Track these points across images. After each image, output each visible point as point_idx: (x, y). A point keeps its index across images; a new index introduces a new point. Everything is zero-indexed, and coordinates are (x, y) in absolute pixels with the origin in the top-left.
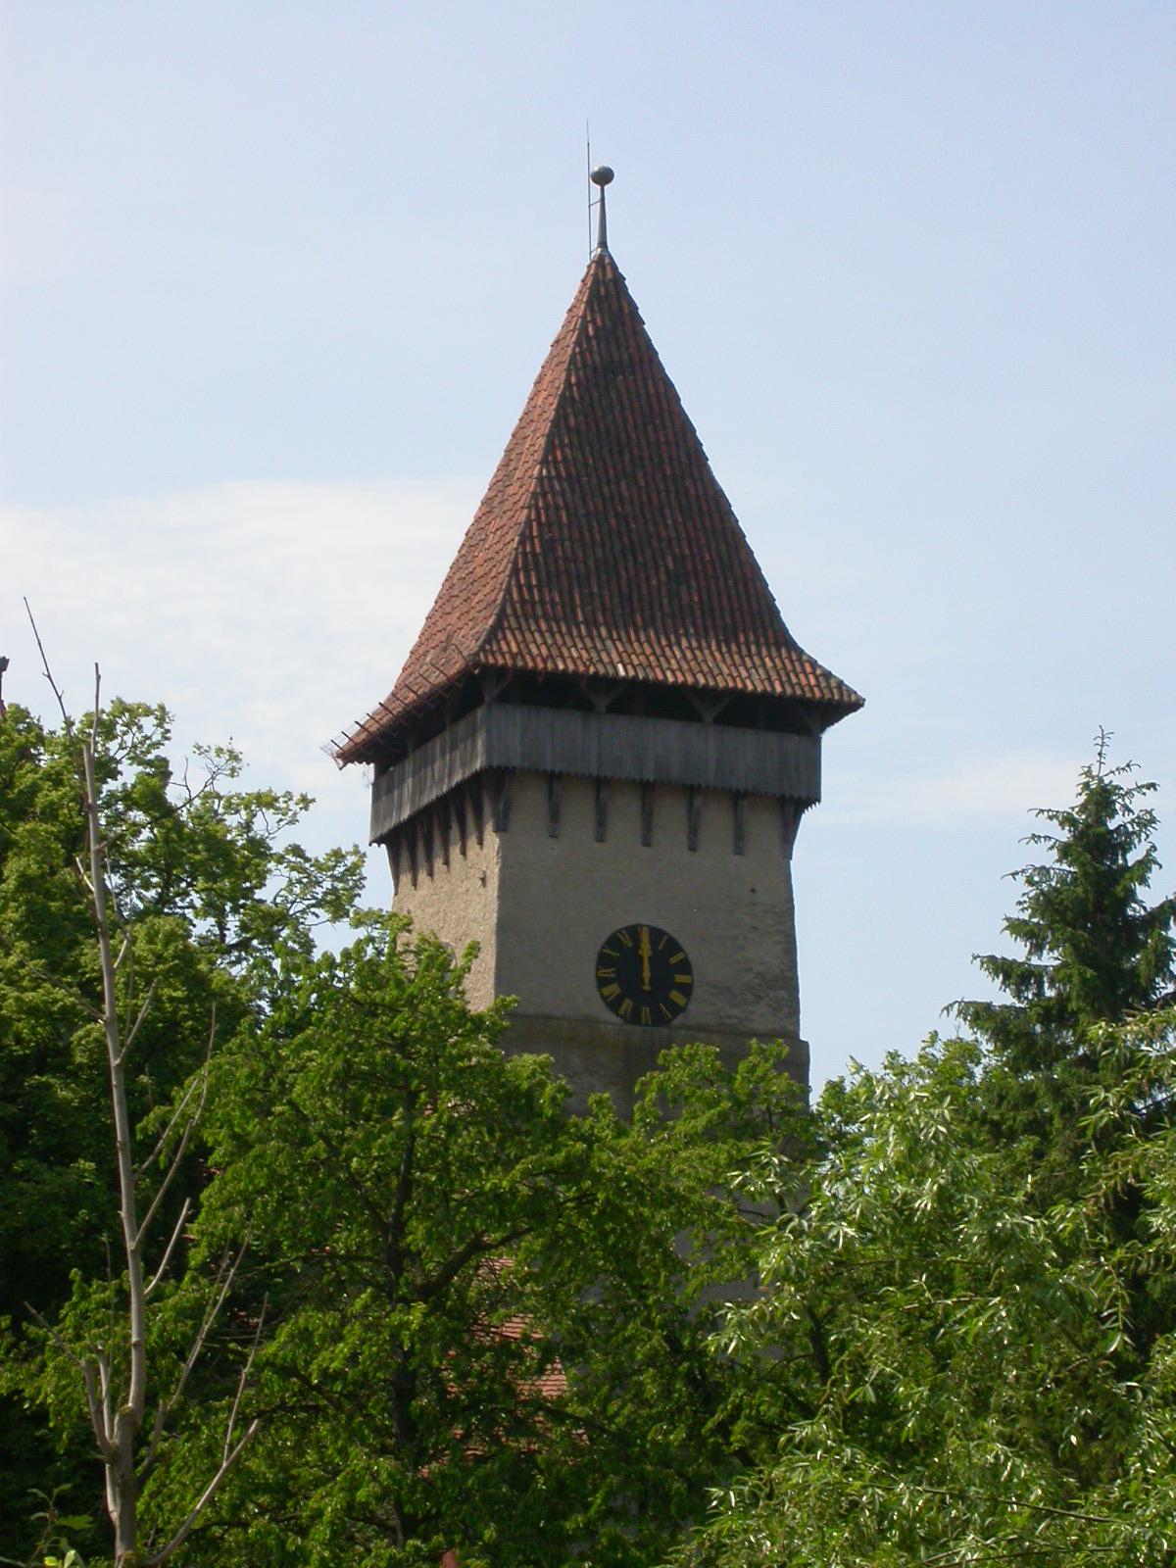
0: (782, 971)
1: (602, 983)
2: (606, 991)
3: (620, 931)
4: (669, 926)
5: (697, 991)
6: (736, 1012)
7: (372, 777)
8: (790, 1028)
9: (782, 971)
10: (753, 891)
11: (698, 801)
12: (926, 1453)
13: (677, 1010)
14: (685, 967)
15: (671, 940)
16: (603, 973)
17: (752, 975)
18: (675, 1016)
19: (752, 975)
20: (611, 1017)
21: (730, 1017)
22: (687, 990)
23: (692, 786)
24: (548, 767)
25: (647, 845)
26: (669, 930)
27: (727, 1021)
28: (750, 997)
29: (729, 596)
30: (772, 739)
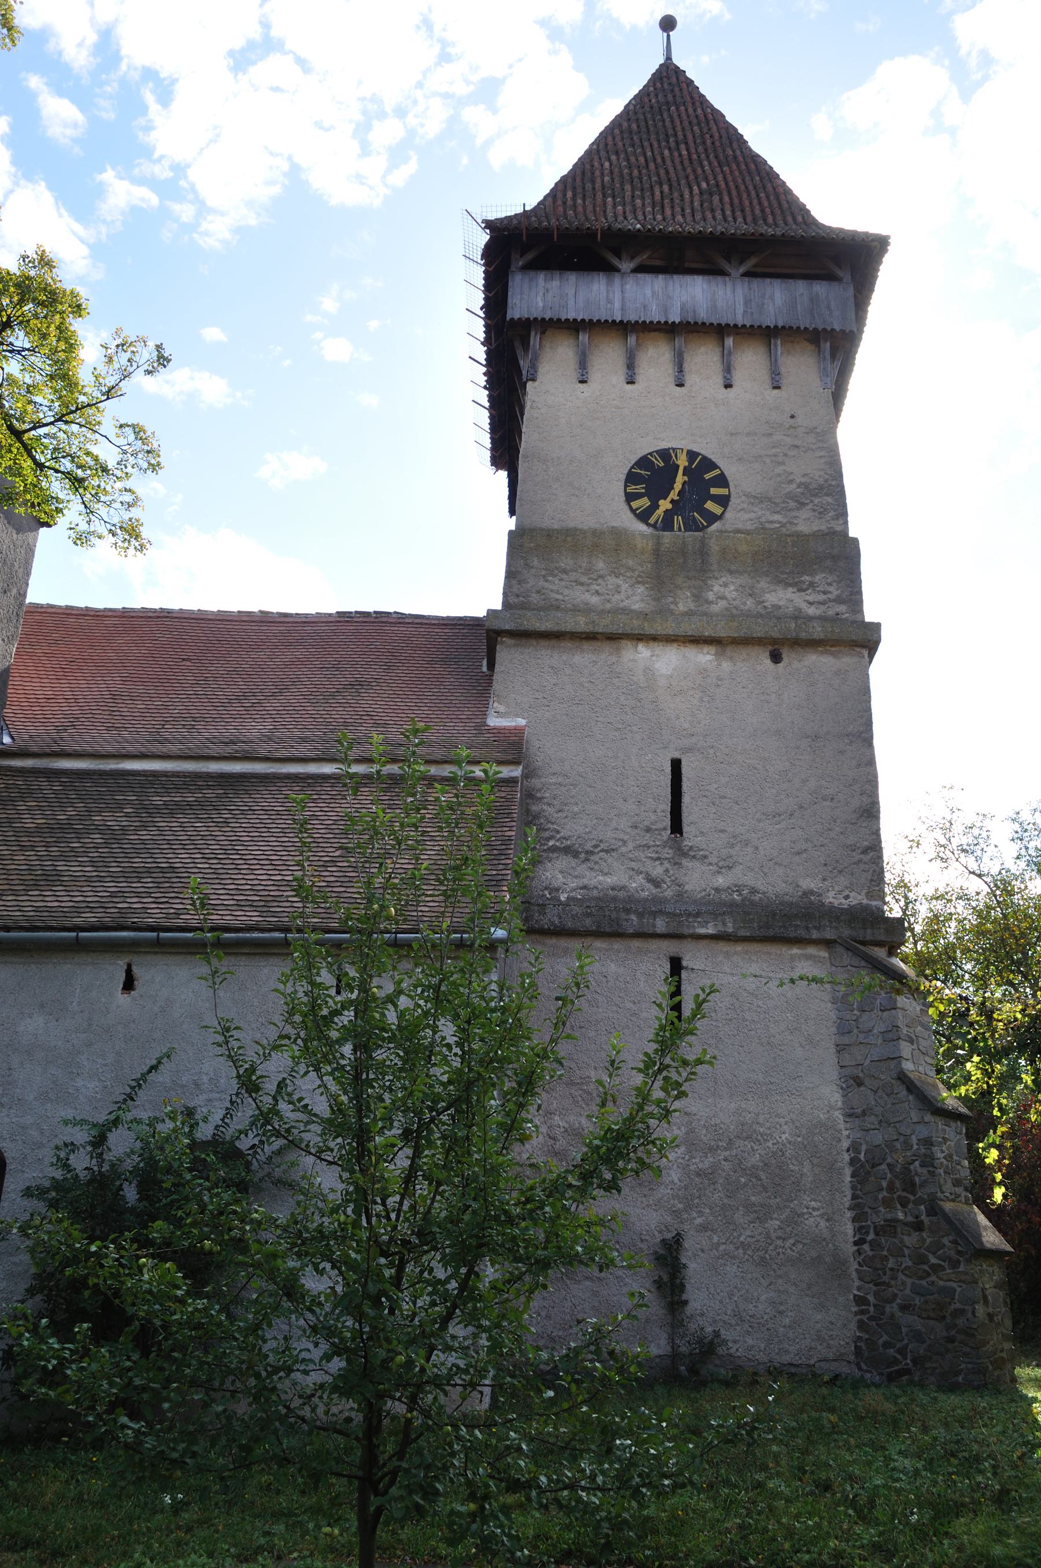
0: (826, 481)
1: (630, 498)
2: (634, 505)
3: (651, 454)
4: (707, 449)
5: (734, 501)
6: (776, 517)
7: (47, 198)
8: (839, 529)
9: (826, 481)
10: (792, 417)
11: (729, 342)
12: (1024, 1421)
13: (713, 518)
14: (722, 481)
15: (705, 459)
16: (716, 509)
17: (794, 486)
18: (710, 524)
19: (794, 486)
20: (642, 527)
21: (772, 522)
22: (723, 501)
23: (719, 325)
24: (571, 316)
25: (680, 385)
26: (703, 452)
27: (767, 525)
28: (792, 504)
29: (750, 173)
30: (800, 287)
